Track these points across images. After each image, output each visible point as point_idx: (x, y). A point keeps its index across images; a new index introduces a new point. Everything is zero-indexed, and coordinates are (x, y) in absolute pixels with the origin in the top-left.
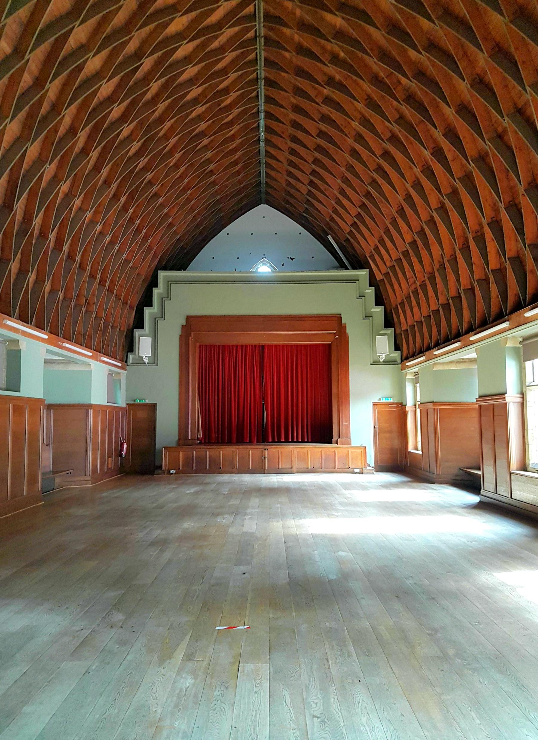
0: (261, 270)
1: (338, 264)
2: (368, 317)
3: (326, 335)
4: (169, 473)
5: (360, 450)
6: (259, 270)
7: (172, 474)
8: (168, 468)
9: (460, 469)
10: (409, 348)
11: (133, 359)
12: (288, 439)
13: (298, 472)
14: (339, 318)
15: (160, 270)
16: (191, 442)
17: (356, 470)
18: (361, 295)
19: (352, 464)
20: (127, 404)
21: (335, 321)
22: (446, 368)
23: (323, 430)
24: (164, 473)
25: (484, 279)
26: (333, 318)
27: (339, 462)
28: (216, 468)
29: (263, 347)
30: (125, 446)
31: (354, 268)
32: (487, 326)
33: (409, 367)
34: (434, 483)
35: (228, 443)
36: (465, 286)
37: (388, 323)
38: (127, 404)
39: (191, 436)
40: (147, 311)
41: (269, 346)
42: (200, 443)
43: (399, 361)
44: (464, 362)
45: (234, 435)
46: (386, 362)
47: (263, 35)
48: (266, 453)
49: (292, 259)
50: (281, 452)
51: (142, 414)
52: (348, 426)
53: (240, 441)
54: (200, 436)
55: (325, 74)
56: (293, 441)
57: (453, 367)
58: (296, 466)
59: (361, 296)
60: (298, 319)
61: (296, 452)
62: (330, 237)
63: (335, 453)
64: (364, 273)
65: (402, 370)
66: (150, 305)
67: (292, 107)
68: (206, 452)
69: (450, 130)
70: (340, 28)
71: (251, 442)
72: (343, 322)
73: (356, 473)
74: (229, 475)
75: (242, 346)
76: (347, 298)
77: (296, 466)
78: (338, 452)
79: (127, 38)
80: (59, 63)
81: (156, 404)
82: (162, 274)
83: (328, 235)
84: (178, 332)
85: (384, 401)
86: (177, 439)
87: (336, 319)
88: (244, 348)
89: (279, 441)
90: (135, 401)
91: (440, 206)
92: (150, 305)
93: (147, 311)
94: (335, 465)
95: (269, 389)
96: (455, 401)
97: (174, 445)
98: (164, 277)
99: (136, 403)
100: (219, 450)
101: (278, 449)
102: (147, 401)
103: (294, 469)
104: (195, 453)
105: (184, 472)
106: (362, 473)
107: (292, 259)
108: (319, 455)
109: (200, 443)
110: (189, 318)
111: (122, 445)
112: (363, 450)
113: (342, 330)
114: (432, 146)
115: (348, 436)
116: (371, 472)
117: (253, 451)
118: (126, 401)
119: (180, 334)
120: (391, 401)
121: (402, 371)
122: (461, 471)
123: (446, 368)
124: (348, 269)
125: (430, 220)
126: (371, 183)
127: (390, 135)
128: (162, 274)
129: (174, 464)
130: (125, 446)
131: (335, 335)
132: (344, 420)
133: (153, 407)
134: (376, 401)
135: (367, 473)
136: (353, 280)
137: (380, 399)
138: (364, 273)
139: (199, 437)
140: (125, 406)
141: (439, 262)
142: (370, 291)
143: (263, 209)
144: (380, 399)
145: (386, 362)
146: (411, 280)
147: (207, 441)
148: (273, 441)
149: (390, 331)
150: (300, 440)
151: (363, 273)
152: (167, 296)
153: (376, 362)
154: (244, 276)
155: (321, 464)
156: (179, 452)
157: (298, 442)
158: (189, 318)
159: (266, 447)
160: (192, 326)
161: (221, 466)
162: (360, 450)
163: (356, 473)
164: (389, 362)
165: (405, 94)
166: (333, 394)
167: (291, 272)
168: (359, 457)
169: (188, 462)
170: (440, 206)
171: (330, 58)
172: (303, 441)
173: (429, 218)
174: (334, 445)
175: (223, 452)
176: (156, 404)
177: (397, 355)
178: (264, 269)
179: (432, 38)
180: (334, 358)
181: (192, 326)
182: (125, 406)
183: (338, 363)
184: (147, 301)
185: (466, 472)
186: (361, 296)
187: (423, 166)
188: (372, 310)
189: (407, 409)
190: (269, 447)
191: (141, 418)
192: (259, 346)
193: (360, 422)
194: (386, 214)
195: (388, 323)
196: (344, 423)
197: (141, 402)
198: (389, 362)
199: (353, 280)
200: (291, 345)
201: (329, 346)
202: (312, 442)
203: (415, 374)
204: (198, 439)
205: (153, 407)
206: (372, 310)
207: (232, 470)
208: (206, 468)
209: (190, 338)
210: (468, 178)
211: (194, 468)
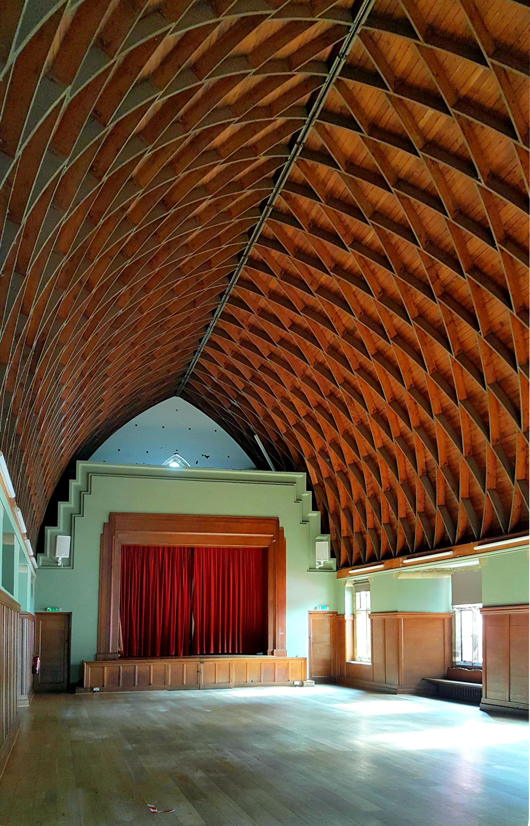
0: (177, 466)
1: (255, 466)
2: (305, 521)
3: (260, 539)
5: (301, 662)
6: (171, 465)
7: (95, 692)
8: (91, 685)
9: (423, 679)
10: (349, 557)
11: (43, 561)
12: (235, 651)
13: (236, 687)
14: (276, 521)
15: (81, 459)
16: (111, 656)
17: (296, 683)
18: (298, 498)
19: (292, 676)
21: (272, 524)
22: (412, 577)
23: (257, 640)
25: (494, 489)
26: (271, 521)
27: (278, 675)
28: (146, 684)
29: (192, 549)
31: (278, 469)
32: (501, 537)
33: (351, 575)
34: (396, 694)
35: (143, 656)
36: (463, 495)
37: (325, 530)
40: (62, 506)
41: (199, 548)
42: (121, 658)
43: (335, 569)
44: (432, 572)
46: (323, 569)
47: (274, 204)
48: (202, 666)
49: (207, 457)
50: (218, 665)
52: (284, 637)
53: (165, 653)
55: (333, 259)
56: (223, 653)
57: (419, 577)
58: (234, 681)
59: (298, 500)
60: (234, 520)
61: (234, 665)
62: (256, 437)
63: (275, 666)
64: (302, 476)
65: (338, 578)
66: (66, 499)
68: (135, 667)
69: (492, 333)
70: (380, 209)
71: (177, 655)
72: (280, 526)
73: (296, 686)
75: (169, 548)
76: (281, 499)
77: (234, 681)
78: (278, 665)
80: (353, 179)
81: (71, 613)
82: (80, 464)
83: (255, 434)
84: (99, 530)
85: (319, 609)
87: (274, 522)
88: (171, 550)
89: (208, 653)
90: (46, 609)
91: (441, 412)
92: (66, 499)
93: (62, 506)
94: (274, 679)
96: (406, 610)
97: (92, 659)
98: (83, 467)
99: (47, 611)
100: (149, 664)
101: (214, 663)
102: (61, 610)
103: (232, 684)
106: (302, 685)
107: (207, 457)
108: (258, 667)
109: (121, 658)
110: (112, 516)
112: (303, 661)
113: (279, 533)
114: (458, 348)
115: (283, 646)
116: (311, 684)
117: (188, 665)
119: (102, 533)
120: (327, 609)
121: (338, 580)
122: (424, 681)
123: (412, 577)
124: (271, 470)
125: (419, 426)
127: (395, 334)
131: (273, 538)
132: (280, 630)
134: (312, 609)
135: (307, 686)
136: (292, 482)
137: (316, 608)
138: (302, 476)
140: (33, 614)
141: (423, 469)
142: (307, 495)
144: (316, 608)
145: (323, 569)
146: (369, 486)
147: (127, 655)
148: (202, 653)
149: (327, 537)
150: (230, 652)
151: (301, 476)
152: (88, 488)
153: (312, 569)
154: (154, 470)
155: (260, 677)
157: (228, 653)
158: (112, 516)
159: (202, 660)
160: (114, 522)
162: (301, 662)
163: (296, 686)
164: (326, 569)
165: (442, 291)
166: (269, 602)
167: (204, 468)
168: (299, 669)
170: (441, 412)
171: (351, 242)
172: (233, 653)
173: (419, 424)
174: (269, 657)
175: (156, 666)
176: (71, 613)
177: (333, 562)
178: (174, 465)
180: (271, 564)
181: (114, 522)
183: (274, 568)
184: (61, 493)
185: (429, 681)
186: (298, 500)
187: (433, 370)
188: (309, 515)
189: (346, 619)
190: (205, 660)
191: (53, 629)
192: (188, 548)
193: (296, 630)
194: (354, 418)
195: (325, 530)
196: (280, 633)
197: (54, 611)
198: (326, 569)
199: (292, 482)
200: (218, 548)
201: (265, 551)
202: (243, 654)
203: (354, 583)
205: (68, 616)
206: (309, 515)
207: (164, 685)
210: (500, 386)
211: (121, 685)
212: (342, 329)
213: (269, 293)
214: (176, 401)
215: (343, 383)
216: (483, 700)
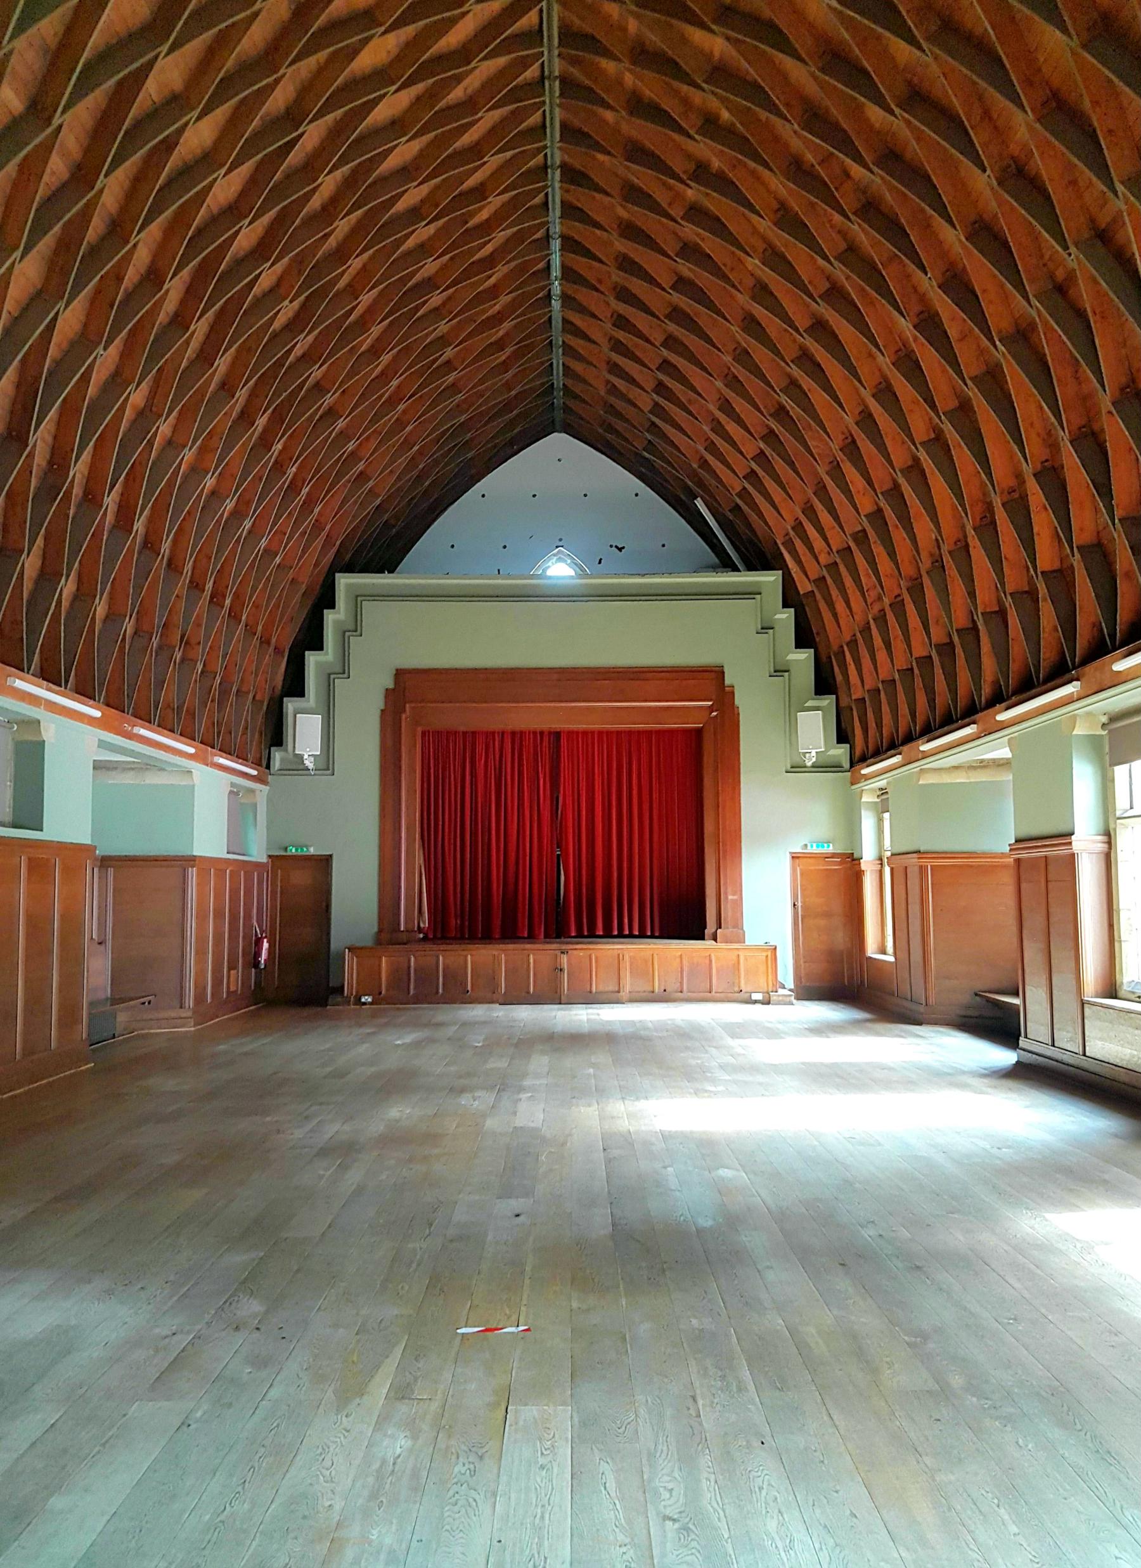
0: (553, 573)
1: (717, 560)
2: (780, 671)
3: (692, 710)
4: (358, 1002)
5: (764, 954)
6: (549, 573)
7: (364, 1004)
8: (357, 992)
9: (976, 995)
10: (867, 737)
11: (282, 760)
12: (611, 930)
13: (632, 1001)
14: (718, 673)
15: (340, 572)
16: (404, 937)
17: (755, 997)
18: (766, 625)
19: (746, 983)
20: (270, 856)
21: (711, 681)
22: (947, 779)
23: (686, 911)
24: (348, 1003)
25: (1026, 592)
26: (706, 675)
27: (718, 978)
28: (458, 993)
29: (557, 735)
30: (266, 945)
31: (751, 567)
32: (1033, 691)
33: (867, 778)
34: (920, 1024)
35: (483, 938)
36: (986, 606)
37: (824, 684)
38: (270, 856)
39: (406, 923)
40: (312, 659)
41: (571, 734)
42: (425, 939)
43: (847, 765)
44: (985, 767)
45: (497, 922)
46: (819, 767)
47: (557, 74)
48: (564, 959)
49: (620, 549)
50: (597, 958)
51: (301, 878)
52: (739, 903)
53: (510, 934)
54: (425, 924)
55: (689, 156)
56: (621, 935)
57: (960, 778)
58: (628, 988)
59: (766, 628)
60: (632, 676)
61: (627, 958)
62: (699, 503)
63: (711, 961)
64: (773, 578)
65: (852, 784)
66: (318, 646)
68: (438, 957)
69: (955, 276)
70: (721, 59)
71: (532, 937)
72: (727, 682)
73: (756, 1002)
74: (486, 1006)
75: (513, 733)
76: (736, 631)
77: (628, 988)
78: (718, 959)
81: (331, 856)
82: (343, 581)
83: (696, 498)
84: (378, 702)
85: (814, 849)
86: (376, 929)
87: (713, 675)
88: (517, 736)
89: (592, 935)
90: (286, 849)
91: (933, 436)
92: (318, 646)
93: (312, 659)
94: (711, 986)
96: (965, 849)
97: (369, 942)
98: (348, 586)
99: (289, 853)
100: (465, 953)
101: (589, 952)
102: (312, 851)
103: (624, 994)
104: (413, 959)
105: (389, 1001)
106: (767, 1002)
107: (620, 549)
108: (676, 964)
109: (425, 939)
110: (400, 674)
111: (259, 942)
112: (769, 953)
113: (724, 699)
114: (917, 308)
115: (738, 924)
116: (788, 999)
117: (536, 956)
118: (268, 849)
119: (383, 707)
120: (830, 849)
121: (854, 787)
122: (978, 998)
123: (947, 779)
124: (737, 570)
125: (911, 467)
127: (828, 285)
128: (343, 581)
129: (369, 982)
130: (266, 945)
131: (711, 709)
132: (729, 890)
133: (324, 863)
134: (798, 849)
135: (779, 1003)
136: (750, 593)
137: (806, 845)
138: (773, 578)
139: (422, 925)
140: (264, 860)
141: (932, 555)
142: (784, 616)
144: (806, 845)
145: (819, 767)
146: (871, 593)
147: (439, 935)
148: (580, 935)
149: (828, 701)
150: (637, 933)
151: (770, 579)
152: (355, 627)
153: (797, 768)
154: (517, 586)
155: (681, 983)
156: (380, 958)
157: (631, 936)
158: (400, 674)
159: (564, 947)
160: (407, 690)
161: (469, 988)
162: (764, 954)
163: (756, 1002)
164: (824, 767)
165: (859, 200)
166: (706, 836)
167: (617, 575)
168: (762, 968)
169: (400, 978)
170: (933, 436)
171: (700, 124)
172: (642, 935)
173: (910, 463)
174: (708, 943)
175: (474, 958)
176: (331, 856)
177: (841, 752)
178: (559, 570)
180: (708, 759)
181: (407, 690)
182: (264, 860)
183: (716, 769)
184: (312, 638)
185: (988, 1000)
186: (766, 628)
187: (897, 352)
188: (788, 658)
189: (863, 867)
190: (571, 947)
191: (299, 885)
192: (550, 733)
193: (764, 894)
194: (819, 454)
195: (824, 684)
196: (730, 897)
197: (299, 852)
198: (824, 767)
199: (750, 593)
200: (618, 732)
201: (699, 732)
202: (662, 936)
203: (879, 793)
204: (420, 930)
205: (324, 863)
206: (788, 658)
207: (492, 996)
208: (437, 992)
209: (404, 716)
210: (993, 377)
211: (412, 992)
212: (750, 282)
213: (619, 226)
214: (558, 443)
215: (787, 387)
216: (1022, 1042)
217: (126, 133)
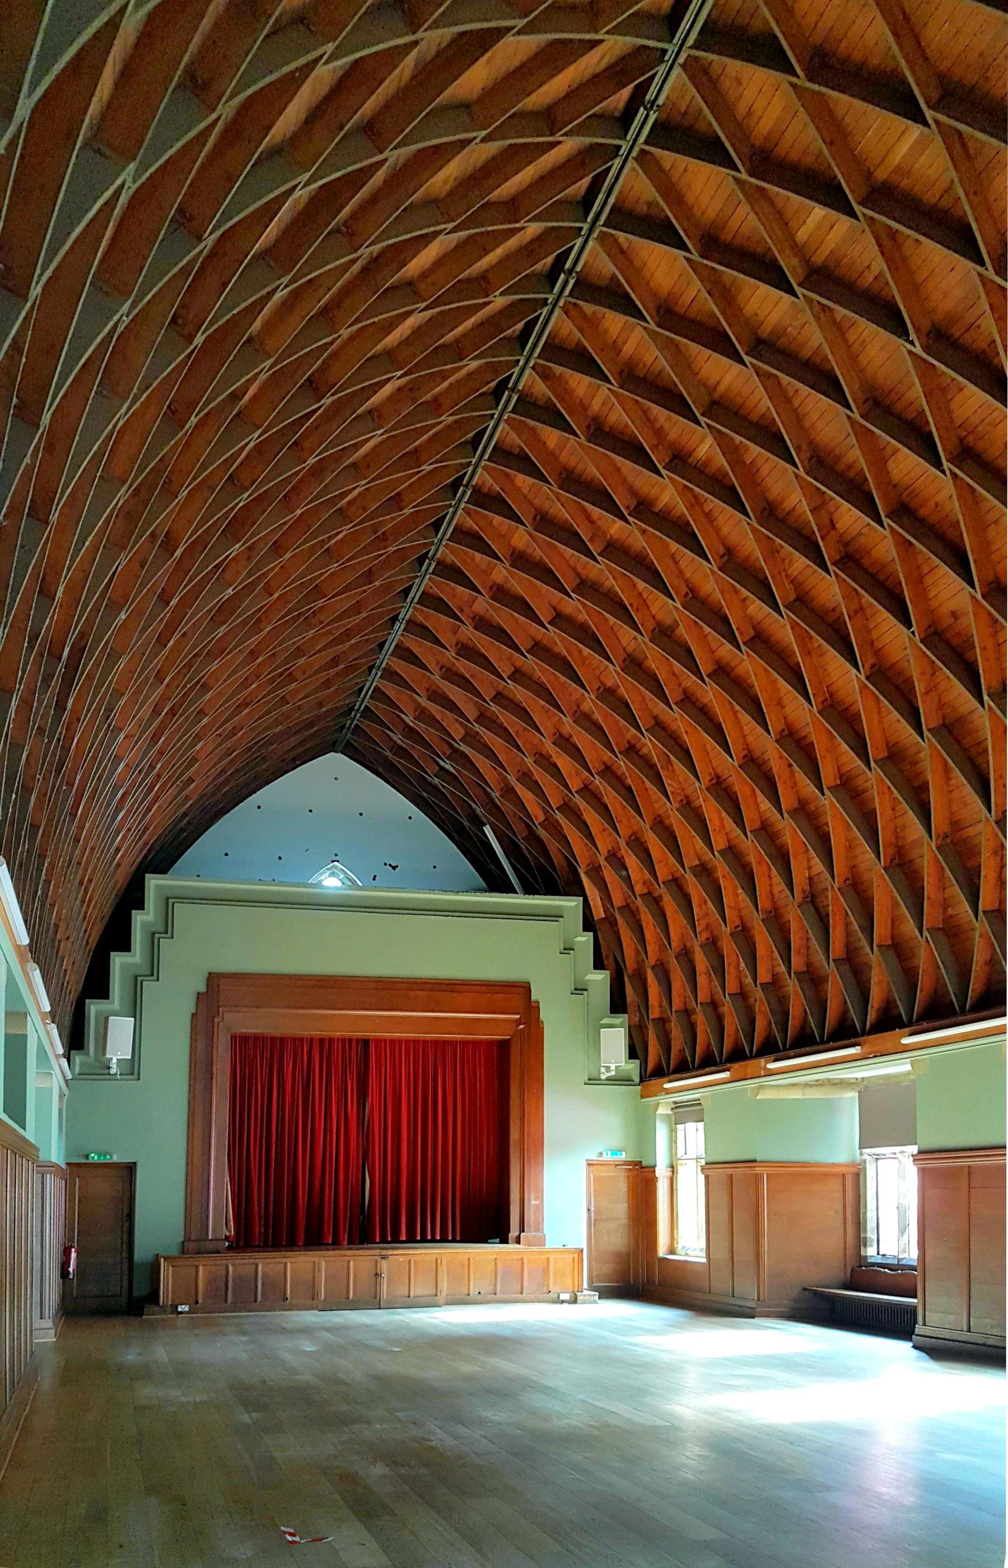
0: (336, 884)
1: (484, 884)
2: (580, 990)
3: (494, 1024)
5: (572, 1256)
6: (325, 883)
7: (181, 1313)
8: (173, 1300)
9: (805, 1289)
10: (664, 1057)
11: (82, 1064)
12: (447, 1236)
13: (449, 1303)
14: (524, 988)
15: (154, 872)
16: (210, 1246)
17: (563, 1297)
18: (567, 946)
19: (555, 1284)
21: (518, 995)
22: (783, 1095)
23: (489, 1215)
25: (939, 929)
26: (515, 990)
27: (529, 1280)
28: (278, 1298)
29: (366, 1042)
31: (530, 890)
32: (953, 1020)
33: (668, 1092)
34: (753, 1317)
35: (273, 1246)
36: (881, 940)
37: (618, 1005)
40: (118, 960)
41: (378, 1041)
42: (230, 1248)
43: (637, 1079)
44: (821, 1085)
46: (614, 1081)
47: (520, 388)
48: (384, 1265)
49: (394, 868)
50: (415, 1262)
52: (540, 1209)
53: (314, 1241)
55: (633, 492)
56: (424, 1240)
57: (796, 1095)
58: (445, 1292)
59: (567, 949)
60: (445, 987)
61: (444, 1262)
62: (487, 830)
63: (523, 1264)
64: (574, 904)
65: (642, 1097)
66: (125, 947)
67: (511, 556)
68: (257, 1266)
69: (936, 633)
70: (722, 396)
71: (336, 1244)
72: (533, 998)
73: (563, 1302)
75: (322, 1041)
76: (534, 948)
77: (445, 1292)
78: (529, 1261)
79: (481, 301)
81: (135, 1163)
82: (153, 881)
83: (485, 825)
84: (188, 1006)
85: (608, 1157)
87: (521, 990)
88: (325, 1044)
89: (396, 1240)
90: (87, 1157)
91: (838, 782)
92: (125, 947)
93: (118, 960)
94: (522, 1288)
95: (376, 1128)
96: (772, 1159)
97: (175, 1252)
98: (157, 886)
99: (90, 1161)
100: (284, 1260)
101: (407, 1258)
102: (115, 1159)
103: (441, 1298)
106: (574, 1301)
107: (394, 868)
108: (490, 1267)
109: (230, 1248)
110: (213, 979)
112: (576, 1256)
113: (531, 1012)
114: (871, 661)
115: (539, 1227)
116: (592, 1298)
117: (357, 1262)
119: (194, 1011)
120: (623, 1156)
121: (643, 1100)
122: (806, 1292)
123: (783, 1095)
124: (515, 892)
125: (797, 809)
126: (653, 727)
127: (752, 633)
131: (518, 1022)
132: (532, 1196)
134: (593, 1156)
135: (584, 1302)
136: (555, 916)
137: (601, 1154)
138: (574, 904)
140: (64, 1166)
141: (804, 891)
142: (584, 939)
143: (335, 762)
144: (601, 1154)
145: (614, 1081)
146: (701, 922)
147: (242, 1244)
148: (384, 1240)
149: (622, 1019)
150: (438, 1238)
151: (572, 904)
152: (167, 927)
153: (593, 1080)
154: (293, 893)
155: (495, 1285)
157: (433, 1240)
158: (213, 979)
159: (384, 1252)
160: (217, 992)
162: (572, 1256)
163: (563, 1302)
164: (621, 1080)
165: (840, 552)
166: (512, 1142)
167: (389, 889)
168: (569, 1270)
170: (838, 782)
171: (667, 460)
172: (444, 1240)
173: (796, 805)
174: (511, 1247)
175: (296, 1265)
176: (135, 1163)
177: (633, 1067)
178: (331, 882)
179: (971, 439)
180: (514, 1072)
181: (217, 992)
183: (522, 1079)
184: (116, 935)
185: (815, 1293)
186: (567, 949)
187: (823, 702)
188: (587, 978)
189: (657, 1174)
190: (390, 1252)
191: (101, 1194)
192: (357, 1040)
193: (564, 1196)
194: (672, 793)
195: (618, 1005)
196: (533, 1202)
197: (102, 1160)
198: (621, 1080)
199: (555, 916)
200: (414, 1041)
201: (504, 1046)
202: (463, 1241)
203: (673, 1106)
205: (130, 1169)
206: (587, 978)
207: (312, 1301)
210: (950, 732)
211: (230, 1300)
217: (672, 339)
